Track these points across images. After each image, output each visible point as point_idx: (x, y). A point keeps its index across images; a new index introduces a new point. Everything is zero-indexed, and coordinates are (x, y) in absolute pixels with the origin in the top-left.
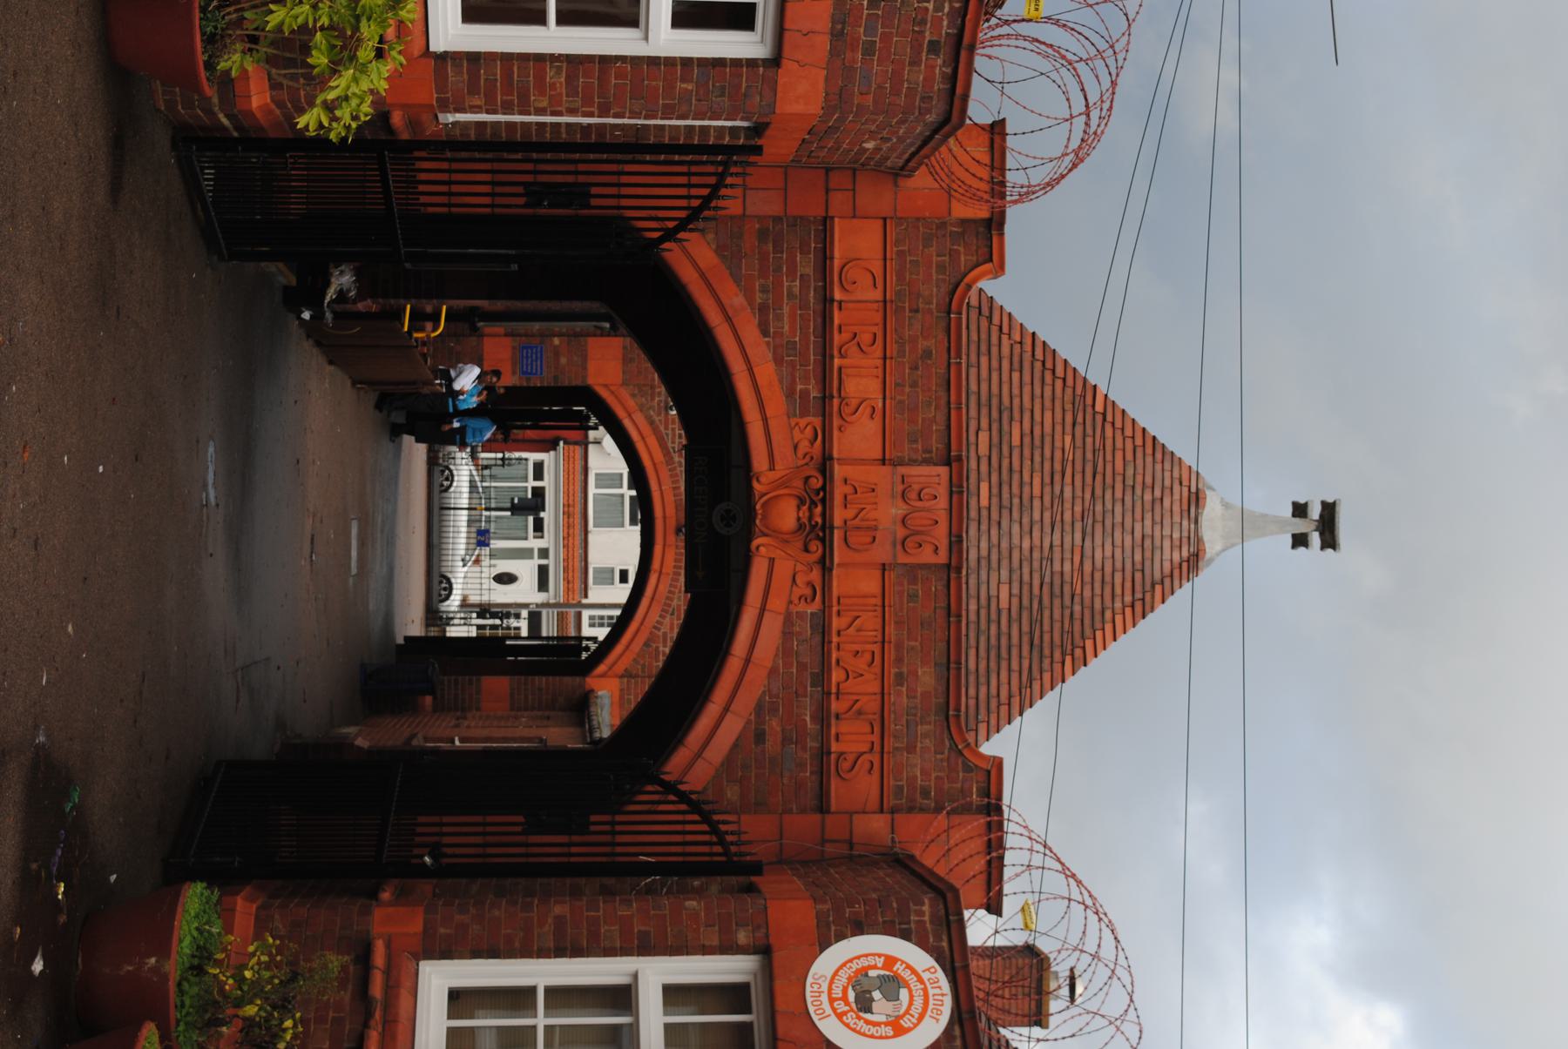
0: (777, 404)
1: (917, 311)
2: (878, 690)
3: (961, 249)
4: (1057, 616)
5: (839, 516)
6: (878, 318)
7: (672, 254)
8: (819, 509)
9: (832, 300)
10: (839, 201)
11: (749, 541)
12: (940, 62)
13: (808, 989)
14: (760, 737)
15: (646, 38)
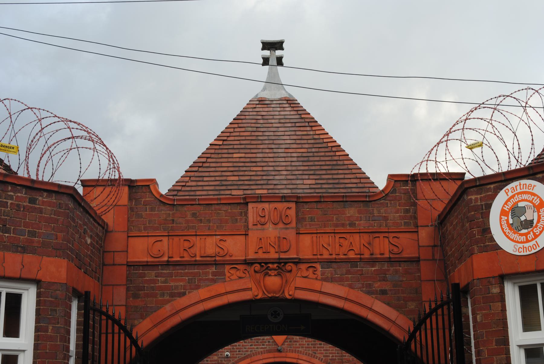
0: (219, 288)
1: (173, 220)
2: (358, 235)
3: (143, 200)
4: (318, 159)
5: (273, 255)
6: (176, 239)
7: (144, 342)
8: (270, 265)
9: (168, 261)
10: (120, 259)
11: (286, 300)
12: (40, 198)
13: (522, 254)
14: (384, 292)
15: (24, 351)
